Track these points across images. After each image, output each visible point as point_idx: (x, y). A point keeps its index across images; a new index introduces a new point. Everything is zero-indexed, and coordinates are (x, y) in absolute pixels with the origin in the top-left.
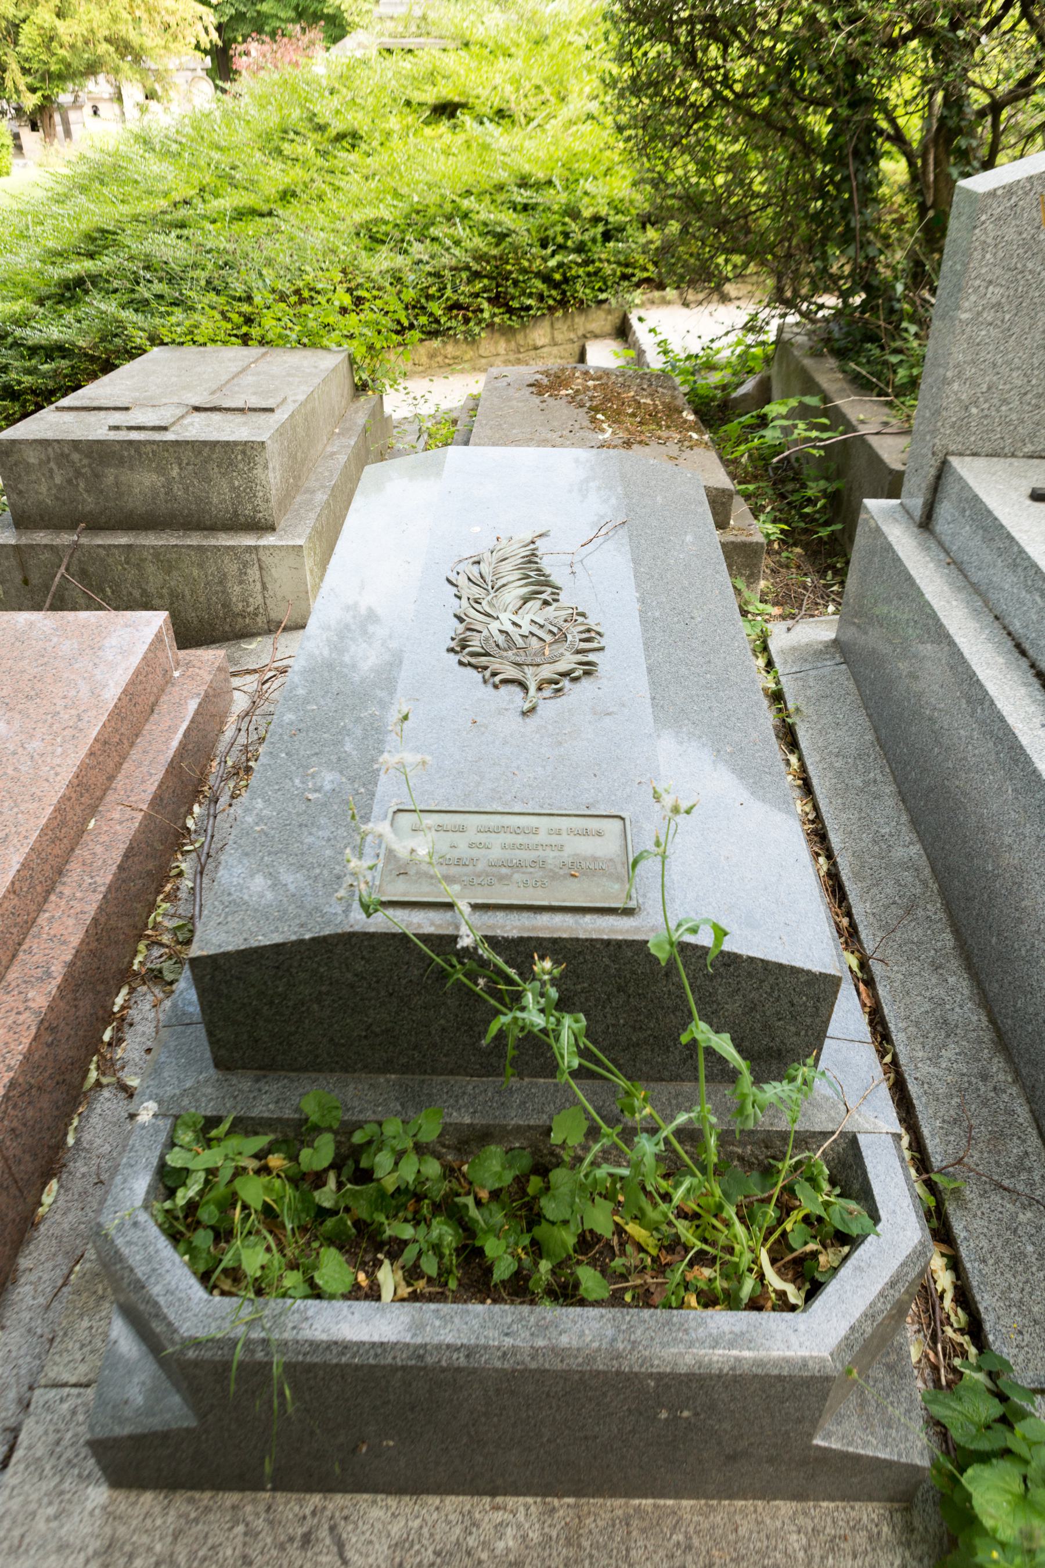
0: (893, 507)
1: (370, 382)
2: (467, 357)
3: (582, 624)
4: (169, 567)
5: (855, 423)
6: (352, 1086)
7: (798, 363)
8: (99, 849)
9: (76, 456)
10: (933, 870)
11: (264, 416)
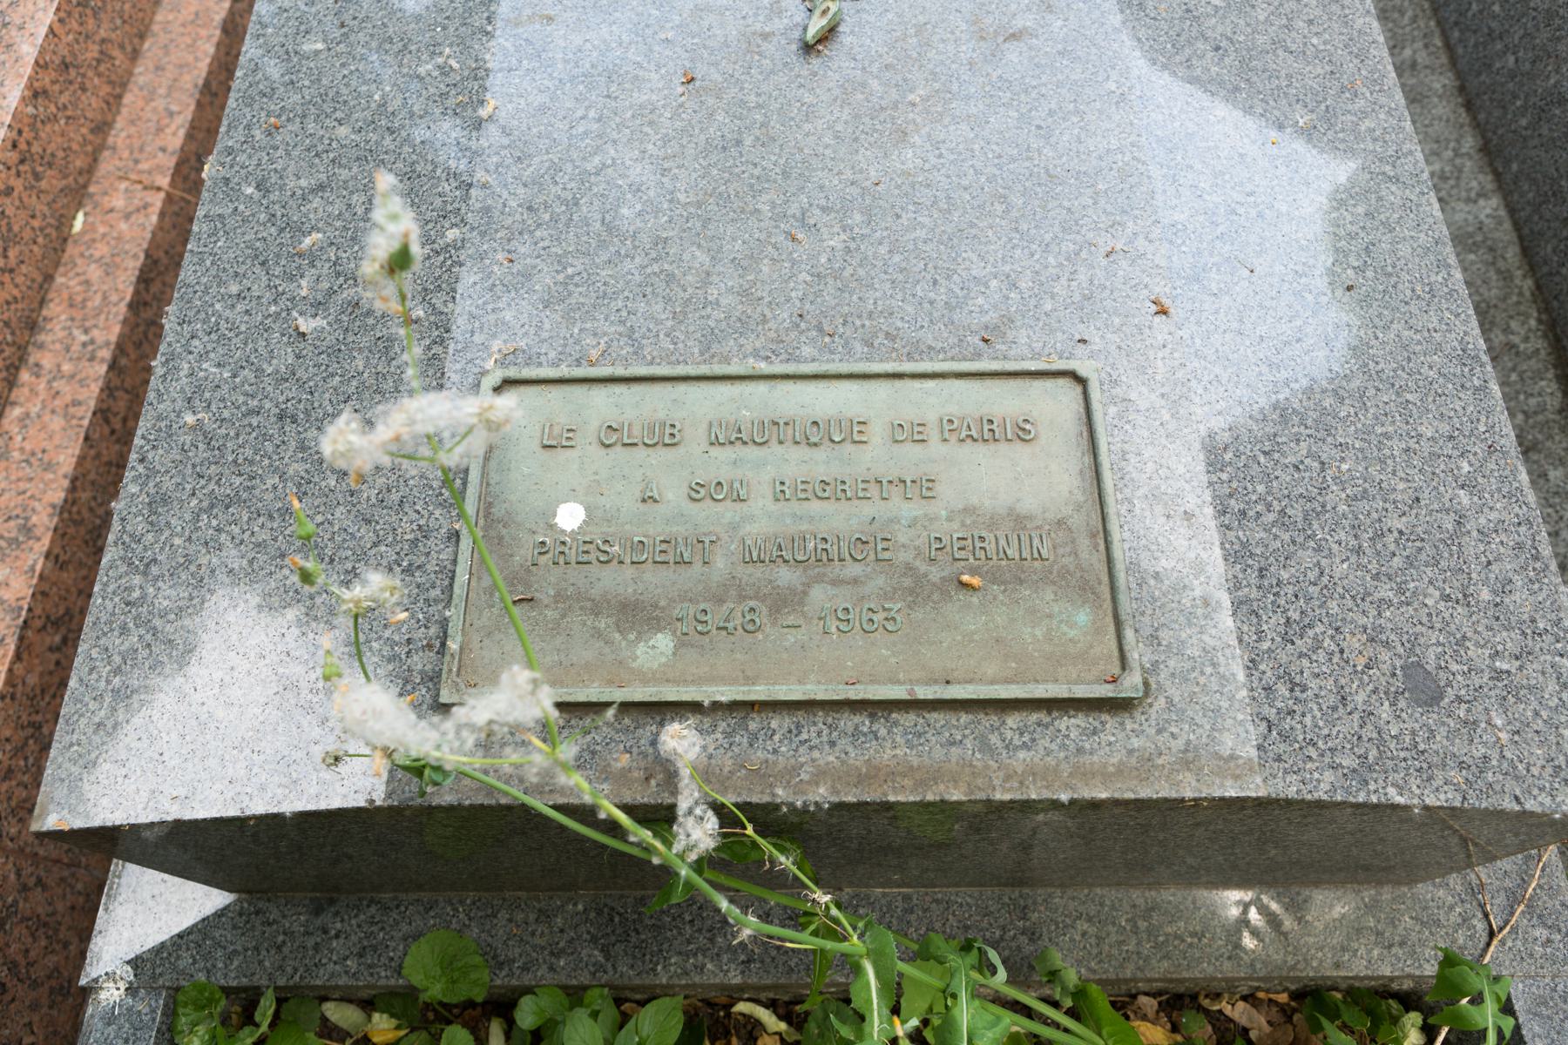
6: (503, 915)
8: (94, 272)
10: (1526, 252)
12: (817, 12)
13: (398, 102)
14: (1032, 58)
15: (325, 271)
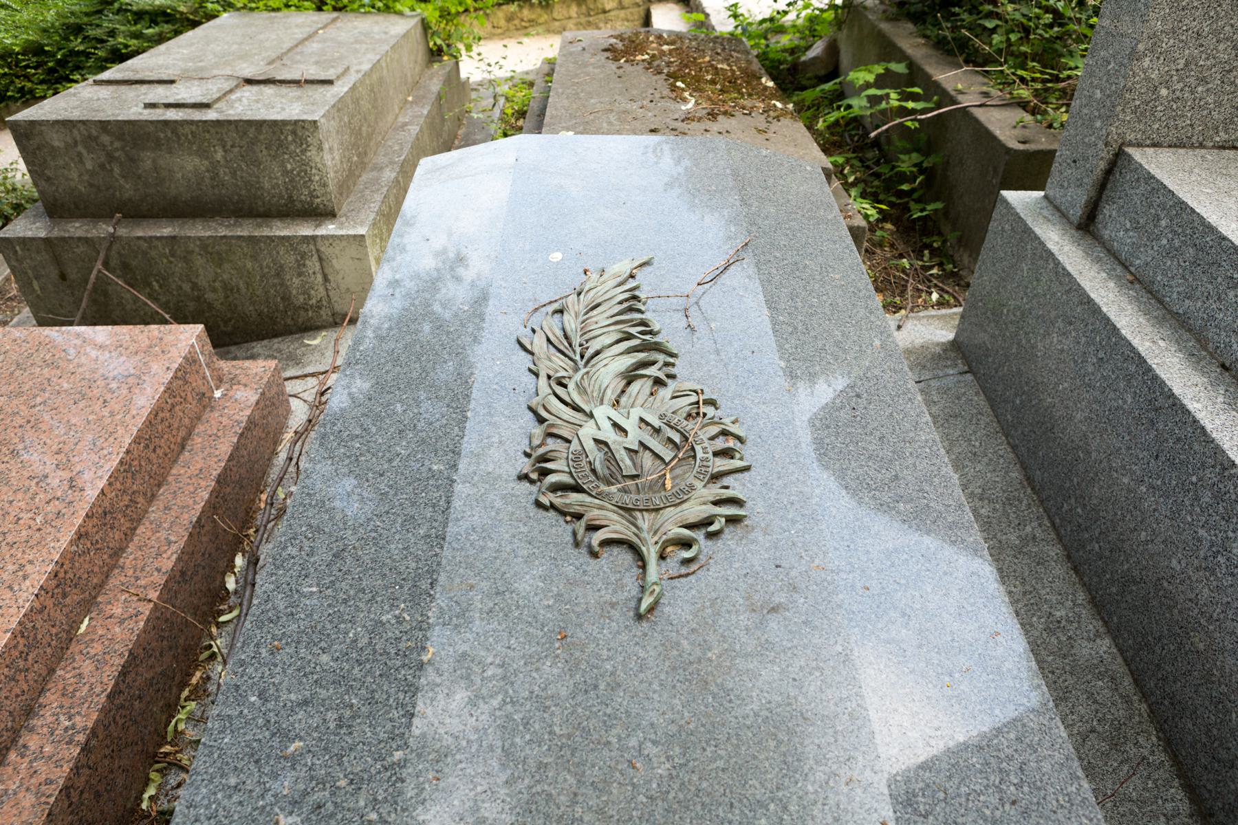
0: (1037, 201)
1: (445, 48)
2: (541, 20)
3: (713, 422)
4: (219, 259)
5: (953, 93)
7: (874, 27)
8: (87, 667)
9: (105, 139)
11: (321, 89)
12: (647, 593)
13: (365, 640)
14: (786, 626)
15: (303, 774)
